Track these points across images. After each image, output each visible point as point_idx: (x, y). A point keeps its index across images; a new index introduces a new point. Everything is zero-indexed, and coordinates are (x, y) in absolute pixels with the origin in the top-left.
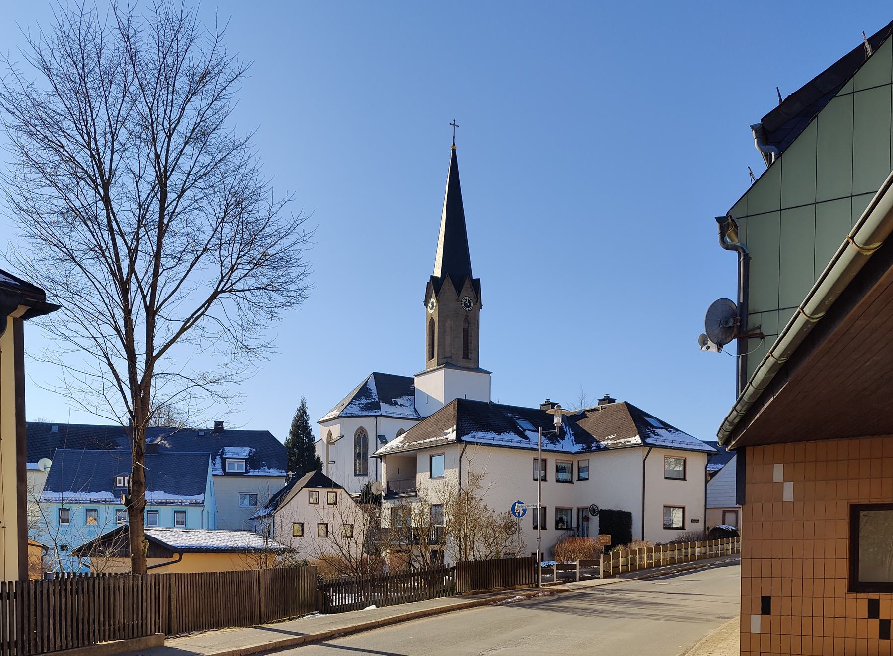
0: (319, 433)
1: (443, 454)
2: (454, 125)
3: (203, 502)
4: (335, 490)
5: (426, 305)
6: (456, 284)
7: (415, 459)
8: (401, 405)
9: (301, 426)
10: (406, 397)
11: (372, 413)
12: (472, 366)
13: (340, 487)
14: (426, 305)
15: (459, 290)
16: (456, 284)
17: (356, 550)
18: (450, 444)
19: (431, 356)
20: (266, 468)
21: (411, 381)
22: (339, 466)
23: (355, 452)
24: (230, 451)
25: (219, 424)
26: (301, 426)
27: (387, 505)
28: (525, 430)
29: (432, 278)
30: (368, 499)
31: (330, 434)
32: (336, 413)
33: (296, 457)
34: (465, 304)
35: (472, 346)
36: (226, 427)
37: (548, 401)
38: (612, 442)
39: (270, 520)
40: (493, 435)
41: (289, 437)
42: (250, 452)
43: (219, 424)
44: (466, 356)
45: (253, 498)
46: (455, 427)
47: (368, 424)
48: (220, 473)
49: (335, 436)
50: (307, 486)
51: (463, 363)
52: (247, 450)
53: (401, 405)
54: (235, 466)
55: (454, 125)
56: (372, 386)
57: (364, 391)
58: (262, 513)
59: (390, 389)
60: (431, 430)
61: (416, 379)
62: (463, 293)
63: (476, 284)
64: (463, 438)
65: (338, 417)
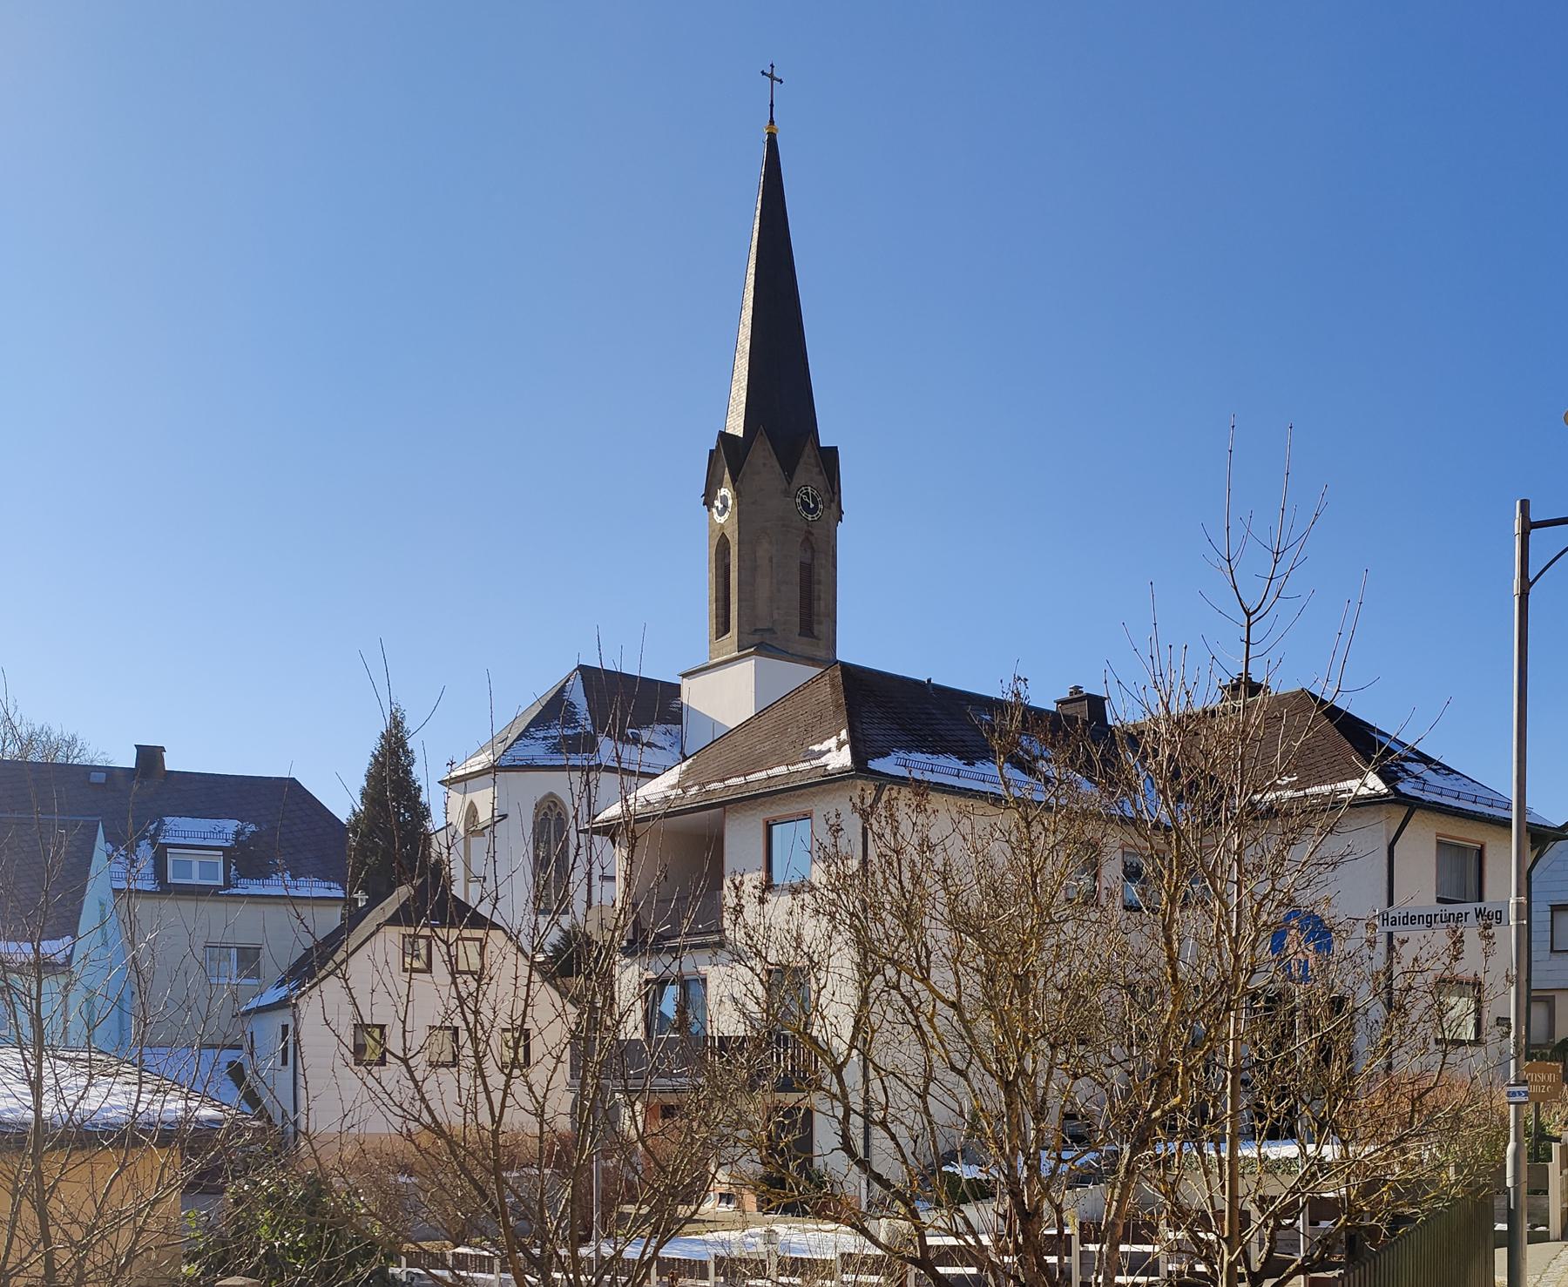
0: (444, 810)
1: (807, 816)
2: (771, 76)
3: (69, 958)
4: (479, 933)
5: (709, 503)
6: (780, 456)
7: (720, 840)
8: (649, 745)
9: (391, 774)
10: (662, 728)
11: (576, 760)
12: (821, 654)
13: (495, 926)
14: (709, 503)
15: (789, 469)
16: (780, 456)
17: (550, 1094)
18: (831, 781)
19: (723, 628)
20: (287, 876)
21: (676, 689)
22: (501, 879)
23: (536, 857)
24: (180, 828)
25: (150, 756)
26: (391, 774)
27: (629, 977)
28: (1036, 759)
29: (724, 436)
30: (570, 964)
31: (472, 811)
32: (485, 759)
33: (384, 853)
34: (805, 505)
35: (820, 607)
36: (172, 763)
37: (1077, 689)
38: (1289, 794)
39: (284, 1017)
40: (955, 763)
41: (359, 807)
42: (238, 833)
43: (150, 756)
44: (807, 629)
45: (249, 958)
46: (844, 734)
47: (562, 785)
48: (148, 885)
49: (484, 816)
50: (394, 921)
51: (802, 645)
52: (232, 825)
53: (649, 745)
54: (196, 870)
55: (771, 76)
56: (578, 696)
57: (555, 708)
58: (271, 996)
59: (616, 708)
60: (767, 746)
61: (686, 684)
62: (801, 477)
63: (829, 458)
64: (874, 765)
65: (494, 769)
